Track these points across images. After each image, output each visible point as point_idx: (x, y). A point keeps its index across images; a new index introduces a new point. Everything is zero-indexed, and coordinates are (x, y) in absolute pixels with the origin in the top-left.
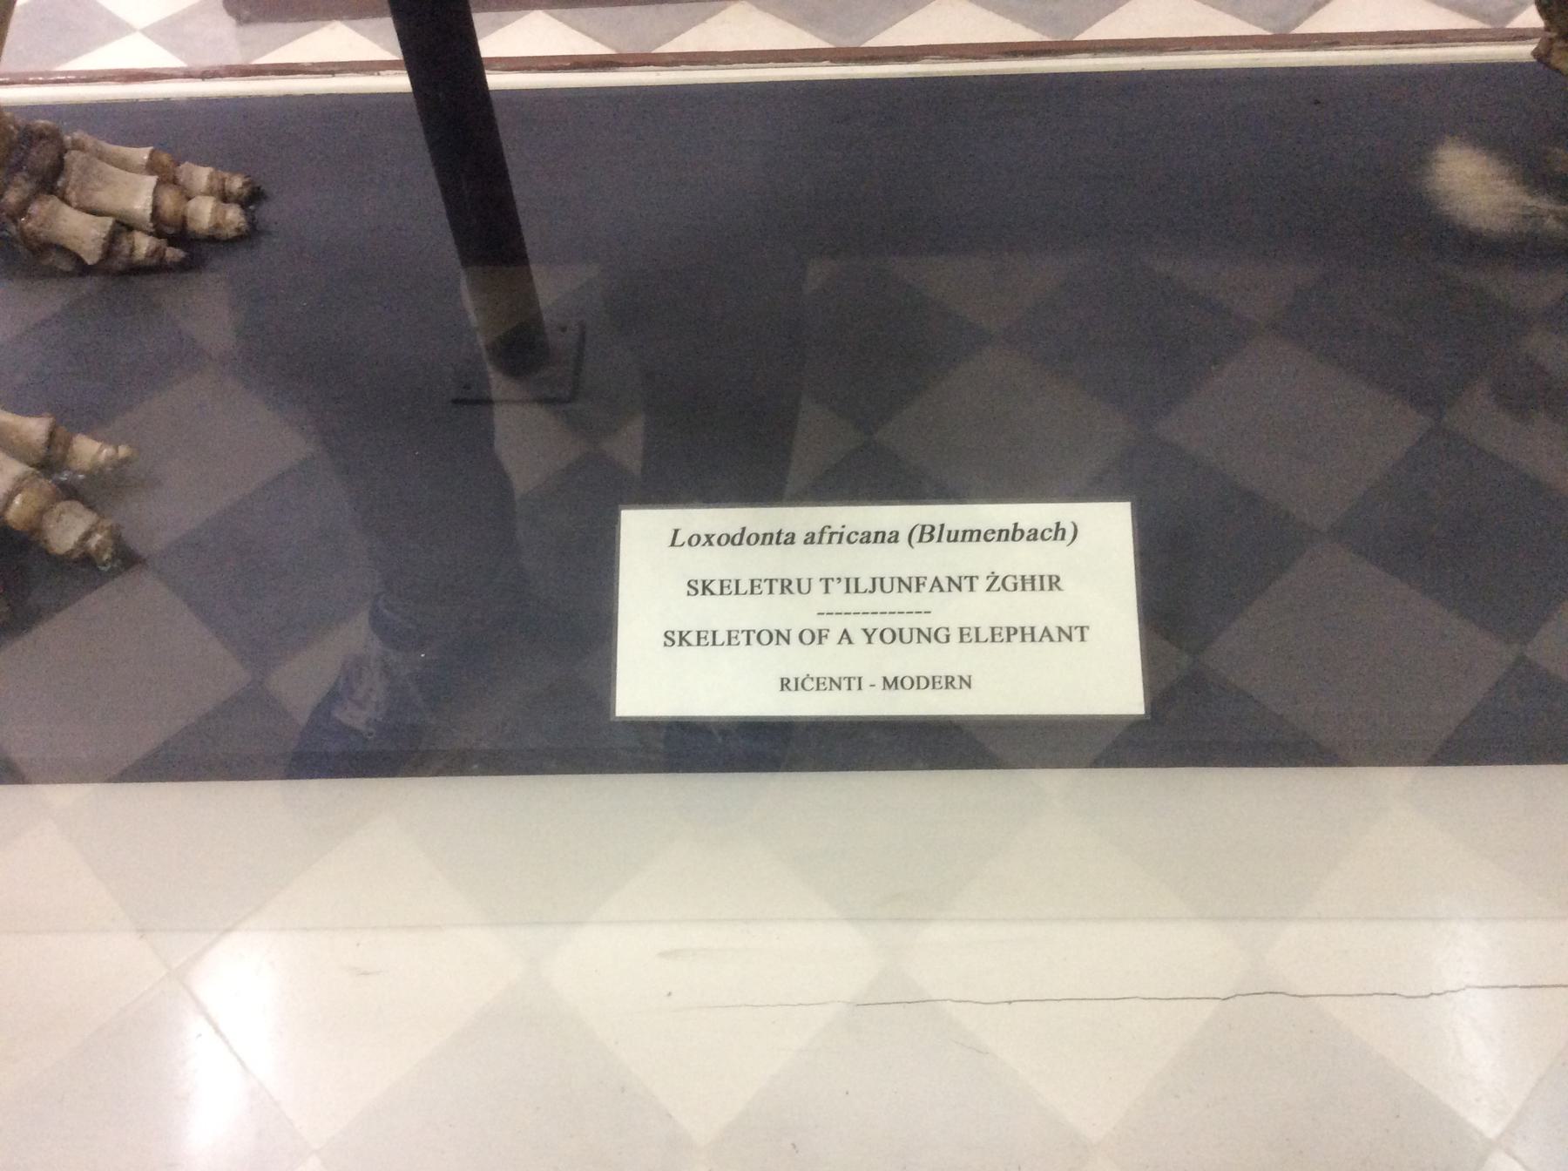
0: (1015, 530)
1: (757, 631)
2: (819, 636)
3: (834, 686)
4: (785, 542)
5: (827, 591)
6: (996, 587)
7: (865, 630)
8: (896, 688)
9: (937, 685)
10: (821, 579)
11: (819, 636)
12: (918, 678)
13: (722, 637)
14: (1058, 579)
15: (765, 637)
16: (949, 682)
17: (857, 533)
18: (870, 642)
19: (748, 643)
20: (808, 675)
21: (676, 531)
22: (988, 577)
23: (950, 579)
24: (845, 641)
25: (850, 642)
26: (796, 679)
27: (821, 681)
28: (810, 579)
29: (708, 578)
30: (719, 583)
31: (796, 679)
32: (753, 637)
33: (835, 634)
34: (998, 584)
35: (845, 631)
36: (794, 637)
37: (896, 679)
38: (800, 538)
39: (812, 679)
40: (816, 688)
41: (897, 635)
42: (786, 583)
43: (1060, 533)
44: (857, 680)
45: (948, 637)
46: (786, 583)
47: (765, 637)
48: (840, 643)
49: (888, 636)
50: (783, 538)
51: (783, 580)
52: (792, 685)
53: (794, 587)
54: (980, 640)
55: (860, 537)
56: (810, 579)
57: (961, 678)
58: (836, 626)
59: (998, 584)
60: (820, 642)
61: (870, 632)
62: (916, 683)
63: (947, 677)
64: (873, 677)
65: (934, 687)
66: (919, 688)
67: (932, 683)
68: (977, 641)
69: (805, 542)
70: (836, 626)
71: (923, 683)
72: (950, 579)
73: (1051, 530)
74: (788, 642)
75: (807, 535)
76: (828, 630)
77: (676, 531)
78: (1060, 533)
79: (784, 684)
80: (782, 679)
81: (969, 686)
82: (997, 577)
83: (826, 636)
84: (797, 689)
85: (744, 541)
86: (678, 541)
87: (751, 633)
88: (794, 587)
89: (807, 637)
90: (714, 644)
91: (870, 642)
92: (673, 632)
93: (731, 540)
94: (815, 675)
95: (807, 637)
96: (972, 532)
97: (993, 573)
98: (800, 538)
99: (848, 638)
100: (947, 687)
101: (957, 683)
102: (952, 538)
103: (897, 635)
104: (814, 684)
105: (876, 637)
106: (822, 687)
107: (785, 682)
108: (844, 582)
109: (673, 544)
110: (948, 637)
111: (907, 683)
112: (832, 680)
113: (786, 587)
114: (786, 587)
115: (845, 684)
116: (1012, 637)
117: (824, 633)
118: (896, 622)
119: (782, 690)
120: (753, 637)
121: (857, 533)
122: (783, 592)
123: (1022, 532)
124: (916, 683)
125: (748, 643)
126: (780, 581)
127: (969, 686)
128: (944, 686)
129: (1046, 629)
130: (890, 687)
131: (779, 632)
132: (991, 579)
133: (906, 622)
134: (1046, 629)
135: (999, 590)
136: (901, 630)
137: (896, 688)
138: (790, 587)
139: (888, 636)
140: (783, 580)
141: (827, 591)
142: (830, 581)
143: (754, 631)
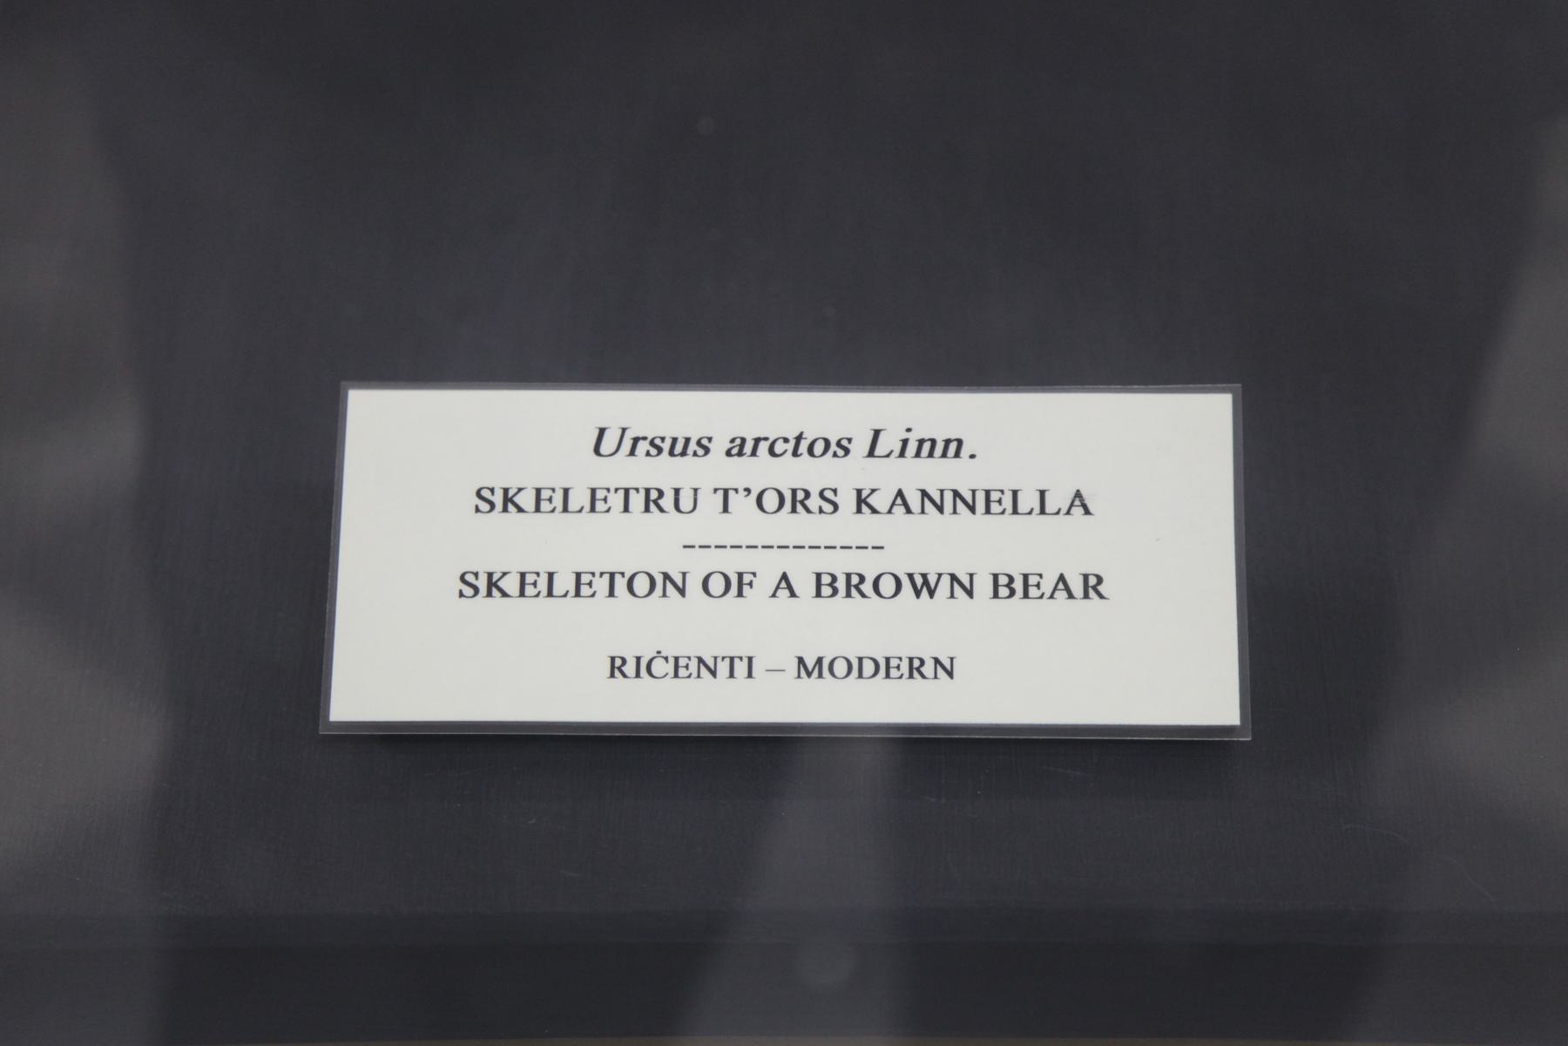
1: (628, 576)
2: (738, 584)
3: (703, 670)
5: (726, 509)
8: (820, 675)
9: (894, 673)
10: (716, 490)
11: (738, 584)
12: (860, 660)
13: (564, 583)
15: (641, 585)
16: (915, 668)
17: (786, 440)
19: (612, 594)
20: (659, 652)
21: (877, 433)
23: (924, 494)
26: (638, 659)
27: (682, 662)
28: (696, 490)
29: (498, 570)
30: (534, 493)
31: (638, 659)
32: (621, 583)
35: (784, 577)
36: (694, 586)
37: (820, 661)
39: (666, 659)
40: (672, 673)
44: (746, 661)
47: (641, 585)
48: (774, 595)
51: (648, 491)
52: (630, 669)
53: (667, 502)
54: (1048, 510)
56: (696, 490)
57: (937, 661)
58: (767, 569)
60: (740, 594)
62: (855, 668)
63: (911, 660)
64: (776, 653)
65: (888, 676)
66: (860, 676)
67: (884, 668)
68: (1015, 511)
69: (728, 453)
70: (767, 569)
71: (869, 667)
72: (924, 494)
75: (733, 441)
76: (754, 574)
77: (877, 433)
79: (616, 667)
80: (613, 659)
81: (950, 674)
83: (750, 584)
84: (638, 675)
87: (618, 578)
88: (667, 502)
89: (717, 585)
90: (550, 594)
92: (476, 575)
94: (671, 653)
95: (717, 585)
98: (719, 446)
99: (790, 587)
100: (911, 676)
101: (928, 669)
104: (670, 667)
106: (682, 672)
107: (618, 662)
109: (871, 454)
111: (840, 667)
112: (700, 660)
115: (723, 668)
117: (747, 578)
119: (612, 675)
120: (621, 583)
122: (647, 510)
124: (855, 668)
125: (612, 594)
126: (642, 492)
127: (950, 674)
128: (906, 674)
129: (1062, 578)
130: (809, 674)
131: (666, 576)
134: (1062, 578)
138: (662, 502)
140: (648, 491)
141: (726, 509)
142: (731, 493)
143: (623, 574)
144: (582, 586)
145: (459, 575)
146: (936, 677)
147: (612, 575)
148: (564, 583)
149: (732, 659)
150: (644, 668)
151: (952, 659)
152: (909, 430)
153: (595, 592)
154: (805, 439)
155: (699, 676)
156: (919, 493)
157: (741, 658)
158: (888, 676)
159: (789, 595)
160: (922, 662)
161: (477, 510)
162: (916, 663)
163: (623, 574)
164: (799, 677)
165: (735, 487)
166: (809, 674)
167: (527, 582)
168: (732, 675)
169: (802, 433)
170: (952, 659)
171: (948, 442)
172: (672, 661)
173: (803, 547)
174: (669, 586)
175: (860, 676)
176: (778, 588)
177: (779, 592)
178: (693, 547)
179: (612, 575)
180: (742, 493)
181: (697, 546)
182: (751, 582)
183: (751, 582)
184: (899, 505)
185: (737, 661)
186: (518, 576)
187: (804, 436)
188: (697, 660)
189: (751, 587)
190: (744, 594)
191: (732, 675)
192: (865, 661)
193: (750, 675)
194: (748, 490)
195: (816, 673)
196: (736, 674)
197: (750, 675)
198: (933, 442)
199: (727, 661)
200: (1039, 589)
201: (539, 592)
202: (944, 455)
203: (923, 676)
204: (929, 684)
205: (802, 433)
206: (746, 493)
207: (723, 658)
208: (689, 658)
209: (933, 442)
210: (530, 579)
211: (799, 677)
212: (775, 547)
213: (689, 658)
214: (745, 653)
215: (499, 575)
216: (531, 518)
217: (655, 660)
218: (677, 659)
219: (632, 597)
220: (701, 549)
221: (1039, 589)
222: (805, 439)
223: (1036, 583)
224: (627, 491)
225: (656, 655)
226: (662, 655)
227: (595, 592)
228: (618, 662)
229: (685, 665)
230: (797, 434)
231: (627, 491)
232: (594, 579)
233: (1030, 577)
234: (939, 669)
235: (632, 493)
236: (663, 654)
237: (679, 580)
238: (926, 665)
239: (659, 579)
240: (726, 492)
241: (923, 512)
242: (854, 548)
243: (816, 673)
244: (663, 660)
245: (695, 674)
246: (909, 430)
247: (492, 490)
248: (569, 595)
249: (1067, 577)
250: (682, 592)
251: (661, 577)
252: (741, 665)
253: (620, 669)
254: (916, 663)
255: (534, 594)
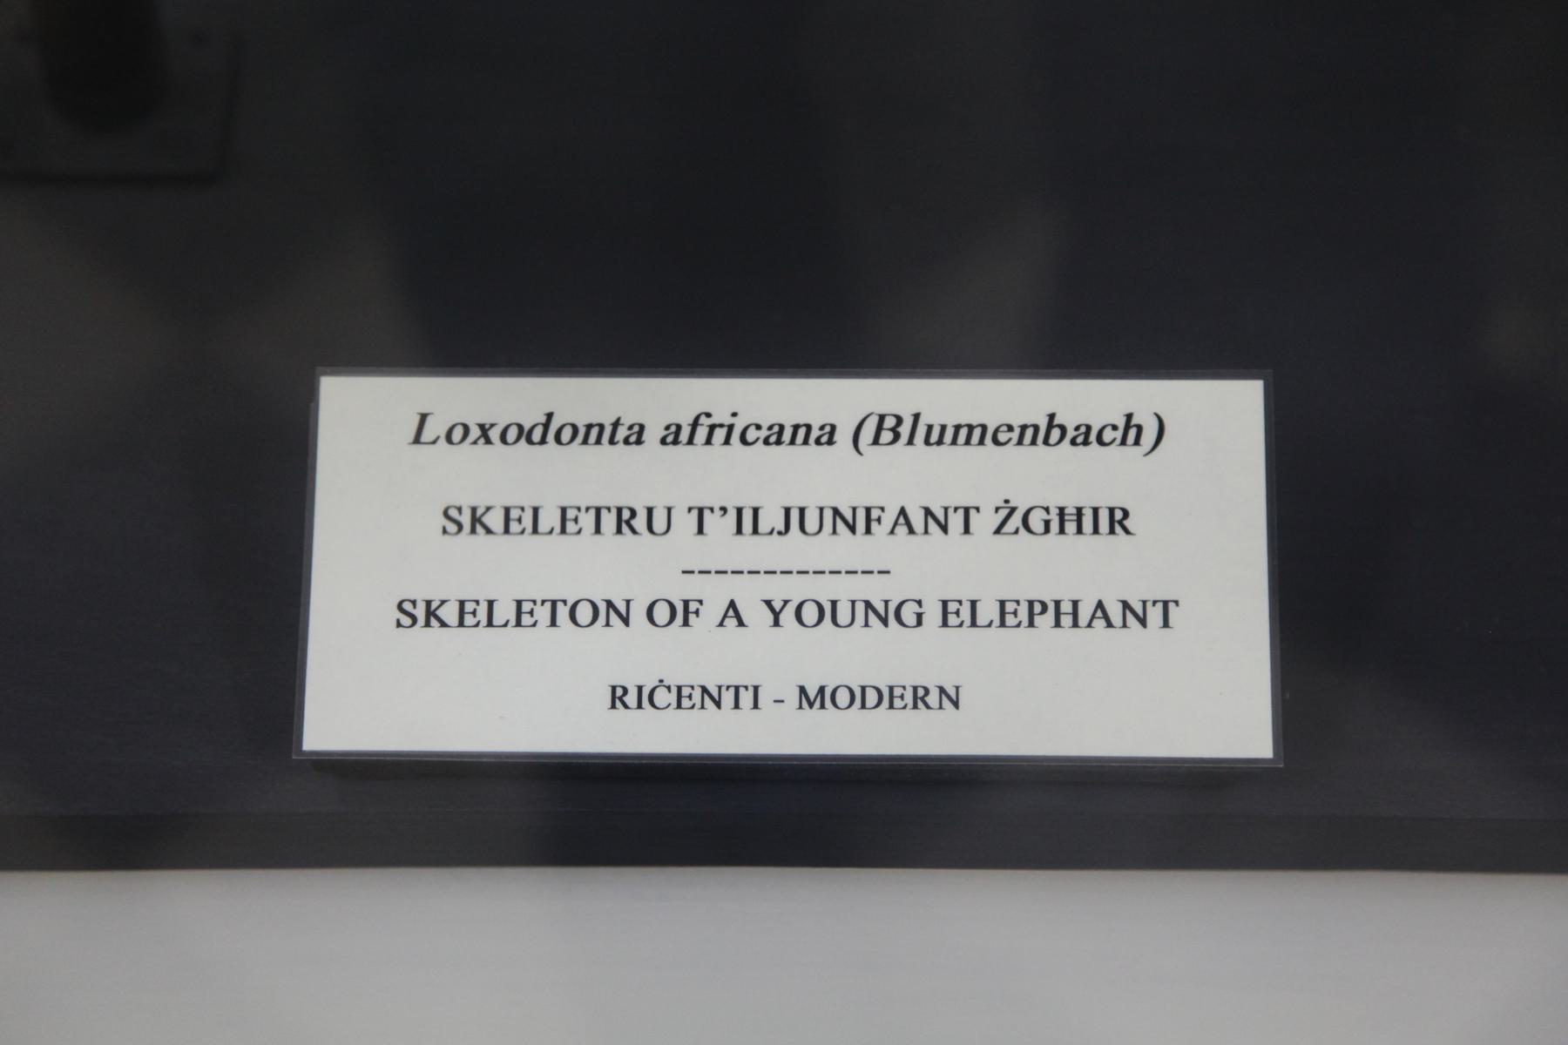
0: (1050, 426)
1: (570, 604)
2: (684, 612)
4: (626, 441)
5: (700, 531)
6: (1010, 527)
7: (768, 603)
8: (822, 706)
9: (898, 703)
10: (690, 510)
11: (684, 612)
12: (863, 689)
13: (505, 612)
14: (1126, 514)
15: (584, 613)
16: (919, 698)
17: (758, 427)
18: (776, 623)
19: (553, 623)
20: (661, 681)
22: (997, 509)
24: (731, 622)
25: (741, 623)
26: (640, 689)
27: (686, 692)
28: (669, 510)
31: (640, 689)
32: (563, 612)
33: (714, 609)
34: (1016, 520)
35: (732, 605)
37: (822, 690)
38: (653, 434)
39: (669, 688)
40: (674, 704)
41: (828, 612)
42: (626, 515)
43: (1132, 433)
44: (751, 690)
45: (919, 616)
46: (626, 515)
47: (584, 613)
48: (721, 624)
49: (810, 613)
50: (622, 433)
52: (631, 699)
53: (640, 523)
55: (764, 433)
56: (669, 510)
57: (942, 690)
58: (715, 594)
59: (1016, 520)
60: (686, 623)
61: (777, 605)
62: (858, 697)
63: (915, 689)
65: (891, 706)
66: (863, 706)
67: (888, 697)
69: (663, 441)
70: (715, 594)
71: (872, 698)
73: (1115, 428)
74: (626, 621)
78: (1132, 433)
79: (617, 697)
80: (614, 688)
81: (956, 704)
82: (1013, 510)
83: (697, 613)
84: (640, 706)
85: (582, 431)
86: (427, 435)
87: (560, 605)
88: (640, 523)
89: (662, 613)
91: (776, 623)
92: (414, 603)
93: (525, 434)
94: (673, 681)
95: (662, 613)
96: (971, 428)
97: (1007, 501)
98: (653, 434)
99: (738, 616)
101: (933, 699)
102: (934, 437)
103: (828, 612)
104: (673, 698)
105: (788, 616)
106: (686, 703)
107: (619, 692)
108: (732, 514)
110: (919, 616)
112: (704, 690)
113: (625, 521)
114: (625, 521)
115: (727, 698)
116: (1037, 619)
117: (693, 606)
118: (824, 590)
119: (613, 706)
120: (563, 612)
121: (758, 427)
122: (619, 531)
123: (1063, 429)
124: (858, 697)
125: (553, 623)
126: (614, 512)
127: (956, 704)
128: (910, 704)
130: (811, 705)
131: (610, 604)
132: (1003, 513)
133: (844, 590)
135: (1016, 532)
136: (834, 603)
137: (822, 706)
138: (634, 523)
139: (810, 613)
140: (619, 510)
141: (700, 531)
142: (707, 513)
143: (565, 602)
144: (949, 615)
145: (396, 603)
146: (941, 708)
147: (554, 603)
148: (505, 612)
149: (737, 688)
150: (647, 698)
151: (957, 688)
152: (734, 415)
153: (536, 622)
154: (623, 424)
155: (703, 707)
156: (923, 512)
157: (746, 688)
158: (891, 706)
159: (737, 624)
160: (927, 691)
161: (445, 531)
162: (921, 692)
163: (565, 602)
164: (801, 707)
165: (710, 505)
166: (811, 705)
167: (466, 610)
168: (737, 706)
169: (619, 419)
170: (957, 688)
171: (796, 428)
172: (674, 690)
173: (766, 572)
174: (612, 614)
175: (863, 706)
176: (725, 616)
177: (727, 621)
178: (839, 572)
179: (554, 603)
180: (718, 512)
181: (778, 572)
182: (698, 610)
183: (698, 610)
184: (902, 524)
185: (742, 690)
186: (457, 604)
187: (621, 422)
188: (700, 689)
189: (698, 616)
190: (690, 623)
191: (737, 706)
192: (868, 690)
193: (756, 706)
194: (724, 510)
195: (818, 704)
196: (741, 705)
197: (756, 706)
198: (927, 442)
199: (732, 690)
200: (532, 616)
201: (1020, 622)
202: (792, 442)
203: (928, 707)
204: (934, 715)
205: (619, 419)
206: (722, 512)
207: (728, 687)
208: (692, 687)
209: (601, 427)
210: (469, 607)
211: (801, 707)
212: (778, 572)
213: (692, 687)
214: (750, 682)
215: (437, 603)
216: (501, 541)
217: (658, 689)
218: (679, 688)
219: (901, 627)
220: (799, 575)
221: (532, 616)
222: (623, 424)
223: (472, 610)
224: (598, 510)
225: (658, 684)
226: (664, 684)
227: (536, 622)
228: (619, 692)
229: (688, 694)
230: (613, 420)
231: (598, 510)
232: (961, 608)
233: (950, 604)
234: (945, 699)
235: (604, 512)
236: (666, 683)
237: (622, 608)
238: (930, 694)
239: (602, 607)
240: (701, 511)
241: (926, 532)
242: (713, 572)
243: (818, 704)
244: (666, 690)
245: (698, 705)
246: (734, 415)
247: (460, 510)
248: (994, 625)
249: (1105, 603)
250: (626, 621)
251: (604, 604)
252: (746, 695)
253: (621, 699)
254: (921, 692)
255: (958, 624)
